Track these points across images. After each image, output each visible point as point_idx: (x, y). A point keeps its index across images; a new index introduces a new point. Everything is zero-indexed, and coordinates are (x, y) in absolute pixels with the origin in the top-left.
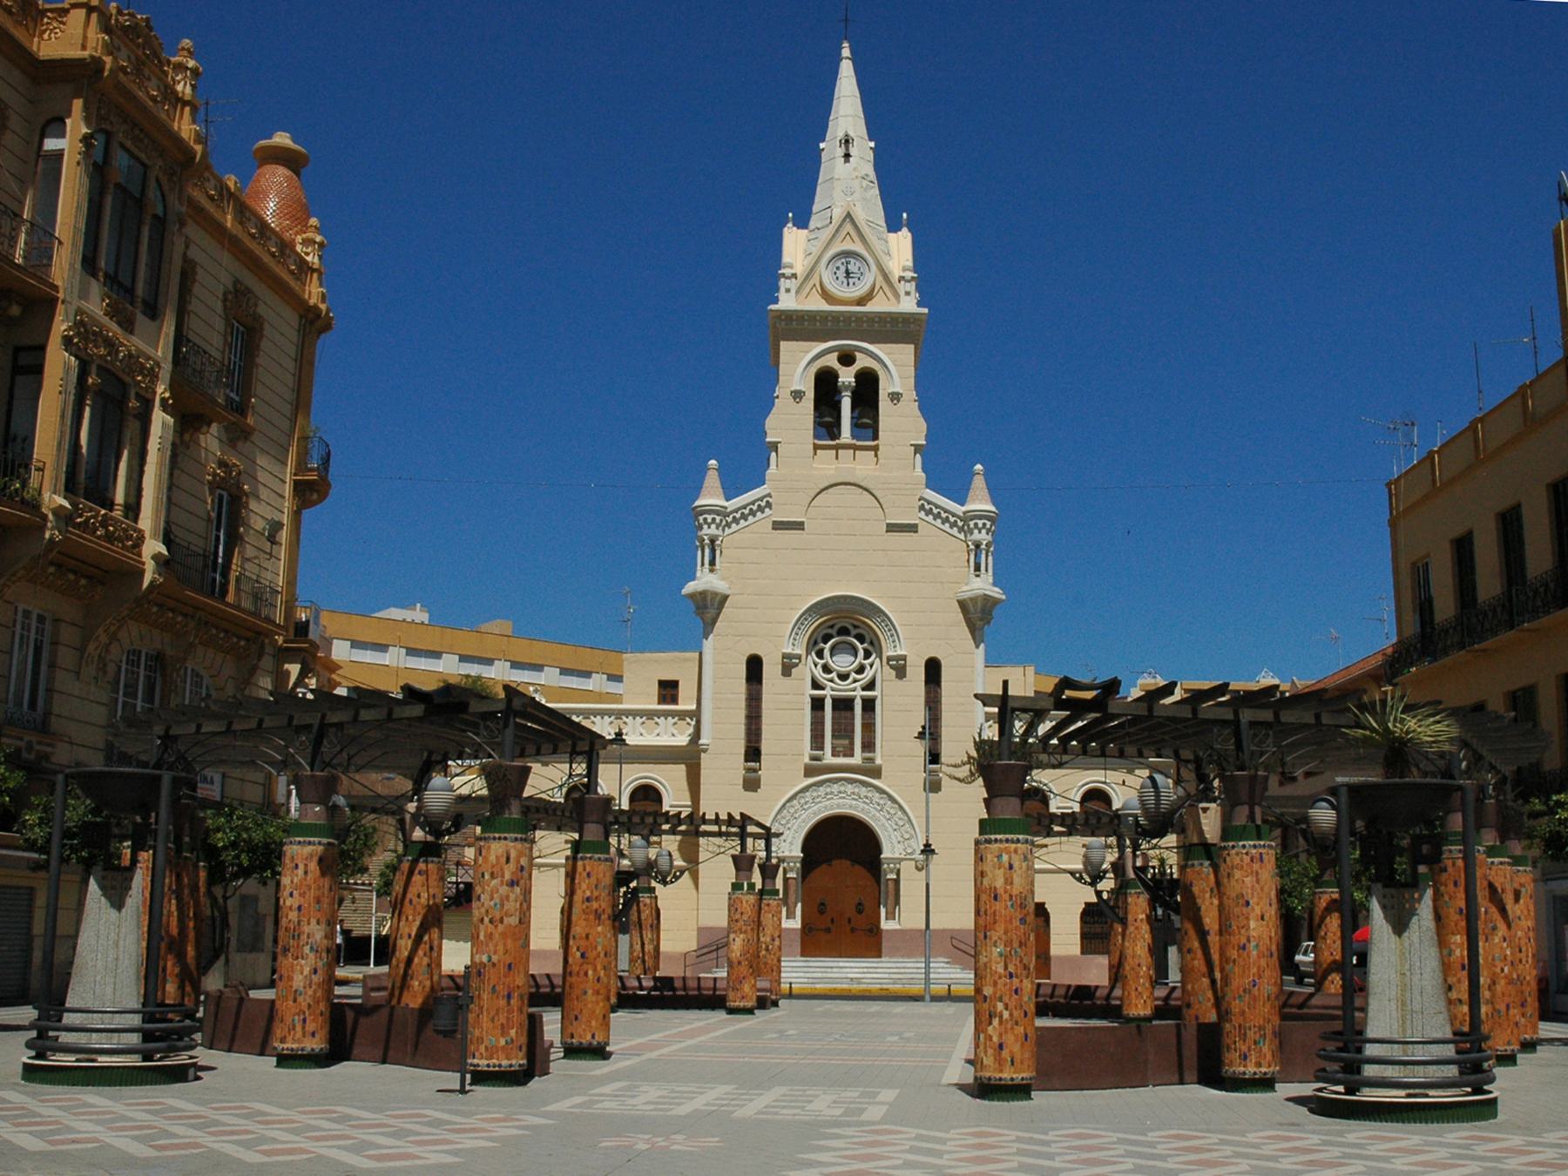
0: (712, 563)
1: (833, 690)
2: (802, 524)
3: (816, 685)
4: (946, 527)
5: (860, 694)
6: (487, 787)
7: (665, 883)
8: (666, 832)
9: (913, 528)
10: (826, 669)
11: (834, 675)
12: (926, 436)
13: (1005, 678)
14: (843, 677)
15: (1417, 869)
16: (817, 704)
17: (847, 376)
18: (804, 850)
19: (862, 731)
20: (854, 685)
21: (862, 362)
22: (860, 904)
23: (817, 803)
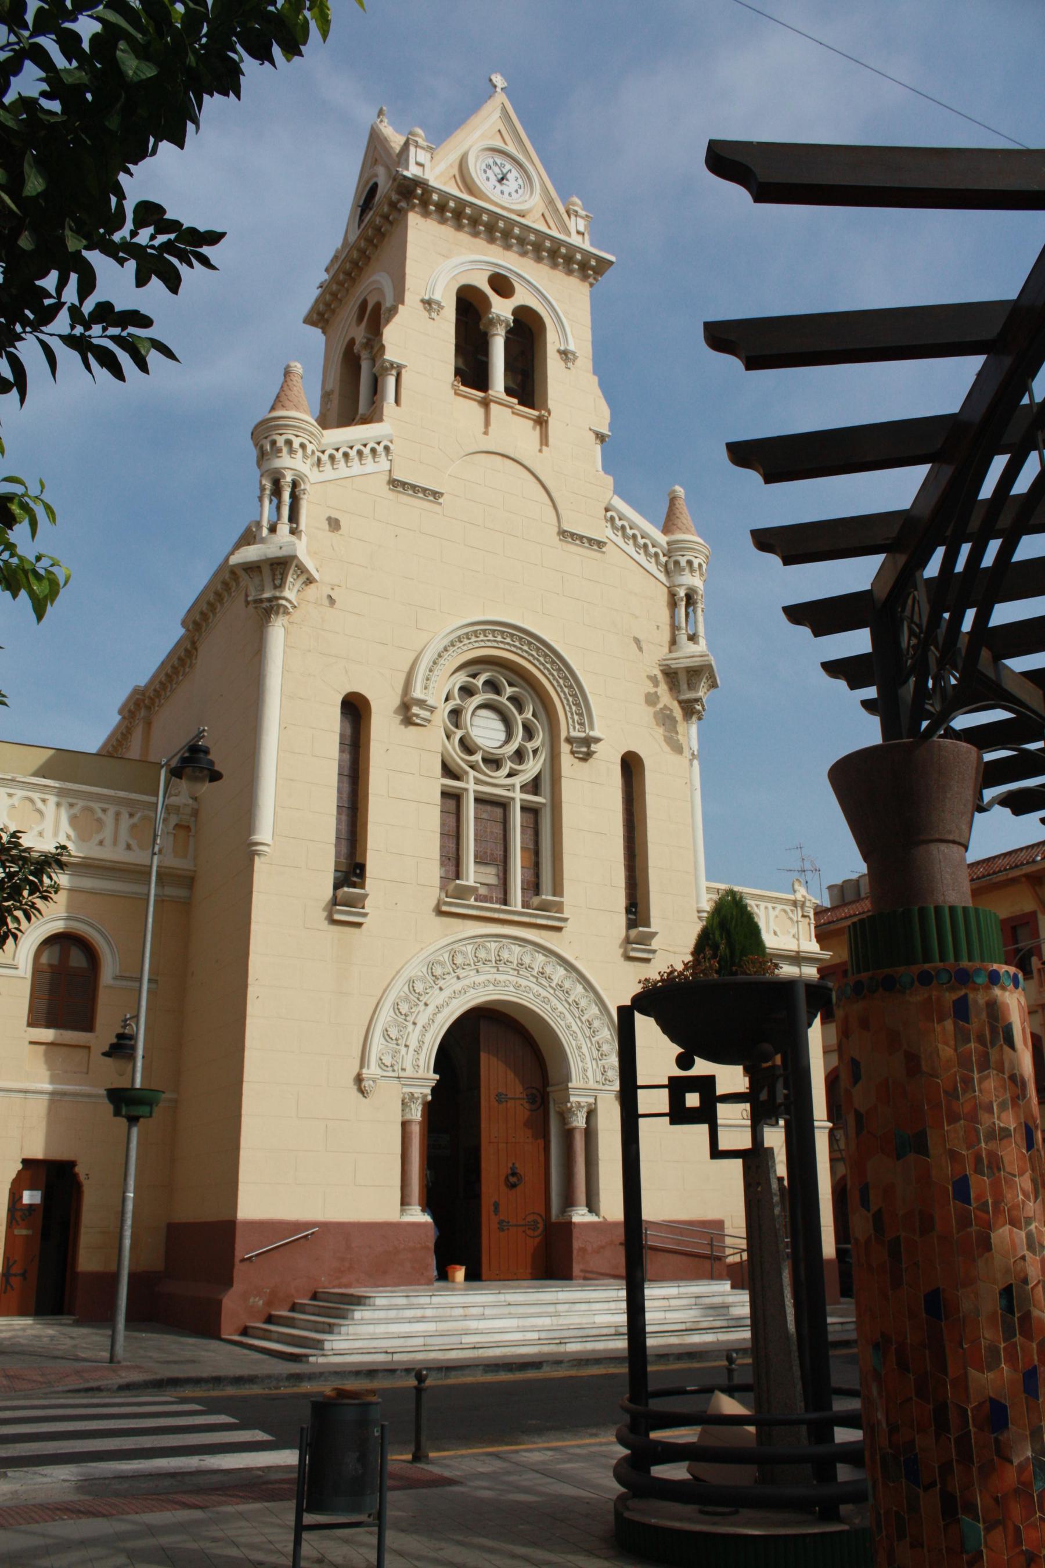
0: (294, 517)
1: (478, 781)
2: (436, 495)
3: (448, 771)
4: (641, 558)
5: (518, 796)
6: (644, 1300)
7: (45, 898)
8: (659, 981)
9: (600, 544)
10: (467, 746)
11: (478, 757)
12: (610, 424)
13: (27, 1043)
14: (493, 762)
15: (683, 1100)
16: (452, 799)
17: (502, 308)
18: (440, 1066)
19: (702, 802)
20: (509, 781)
21: (522, 297)
22: (513, 1186)
23: (519, 975)
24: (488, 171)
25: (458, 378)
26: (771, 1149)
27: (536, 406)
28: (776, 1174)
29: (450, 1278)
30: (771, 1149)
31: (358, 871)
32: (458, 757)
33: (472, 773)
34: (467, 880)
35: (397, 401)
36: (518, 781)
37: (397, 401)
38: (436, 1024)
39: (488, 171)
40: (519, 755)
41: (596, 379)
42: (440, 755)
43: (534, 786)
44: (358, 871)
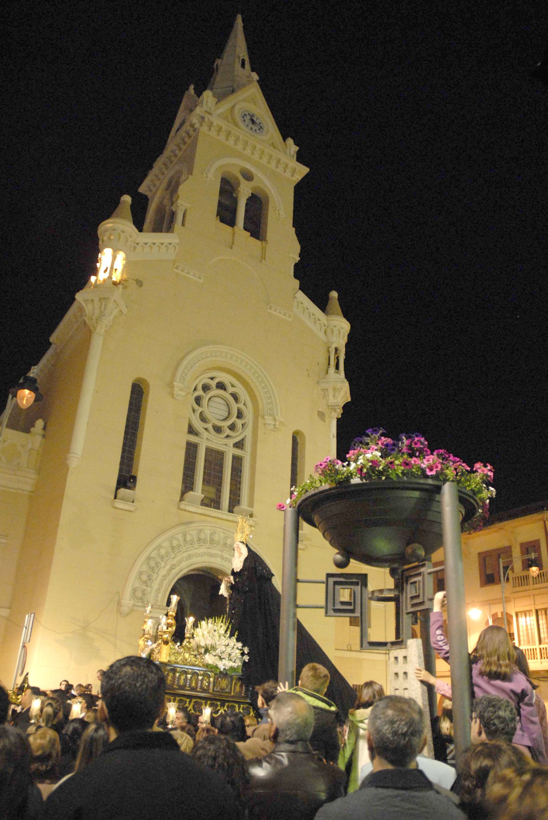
3: (191, 430)
24: (245, 117)
25: (218, 216)
26: (50, 344)
27: (261, 237)
28: (446, 790)
29: (194, 490)
30: (50, 344)
31: (132, 481)
32: (198, 425)
33: (206, 433)
34: (197, 493)
35: (183, 224)
36: (232, 442)
37: (183, 224)
38: (170, 576)
39: (245, 117)
40: (232, 427)
41: (294, 229)
42: (188, 420)
43: (239, 445)
44: (132, 481)
